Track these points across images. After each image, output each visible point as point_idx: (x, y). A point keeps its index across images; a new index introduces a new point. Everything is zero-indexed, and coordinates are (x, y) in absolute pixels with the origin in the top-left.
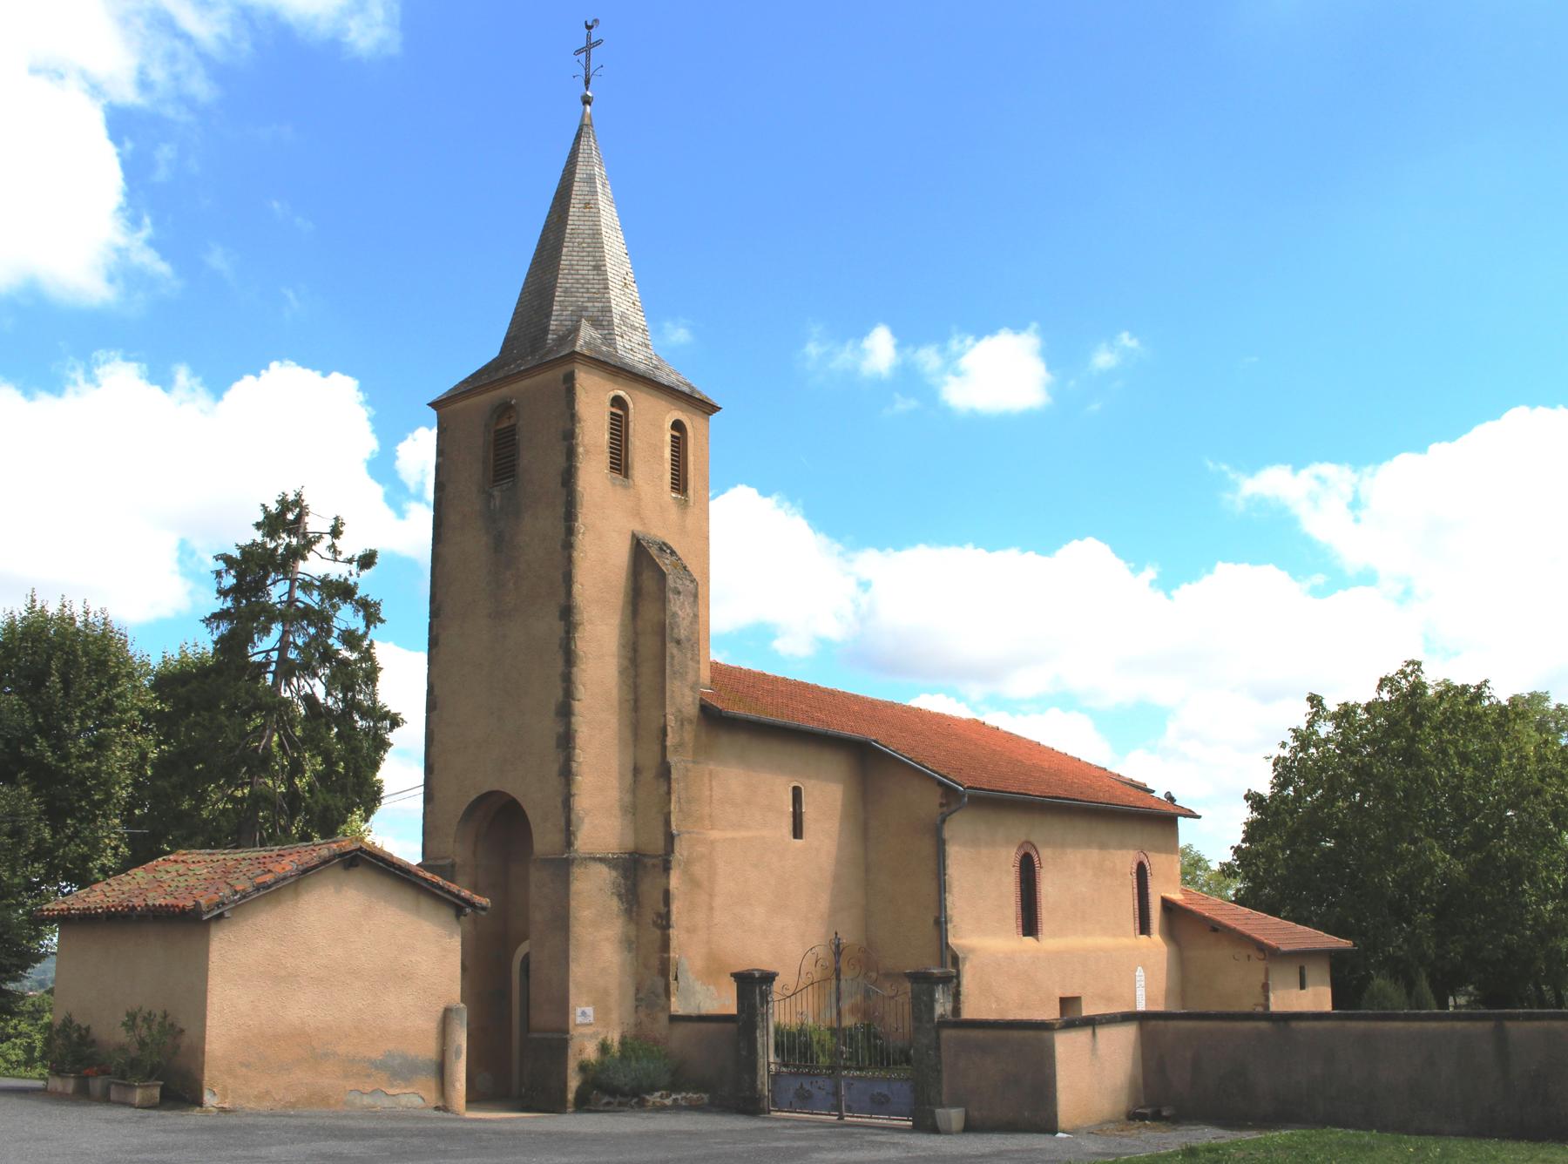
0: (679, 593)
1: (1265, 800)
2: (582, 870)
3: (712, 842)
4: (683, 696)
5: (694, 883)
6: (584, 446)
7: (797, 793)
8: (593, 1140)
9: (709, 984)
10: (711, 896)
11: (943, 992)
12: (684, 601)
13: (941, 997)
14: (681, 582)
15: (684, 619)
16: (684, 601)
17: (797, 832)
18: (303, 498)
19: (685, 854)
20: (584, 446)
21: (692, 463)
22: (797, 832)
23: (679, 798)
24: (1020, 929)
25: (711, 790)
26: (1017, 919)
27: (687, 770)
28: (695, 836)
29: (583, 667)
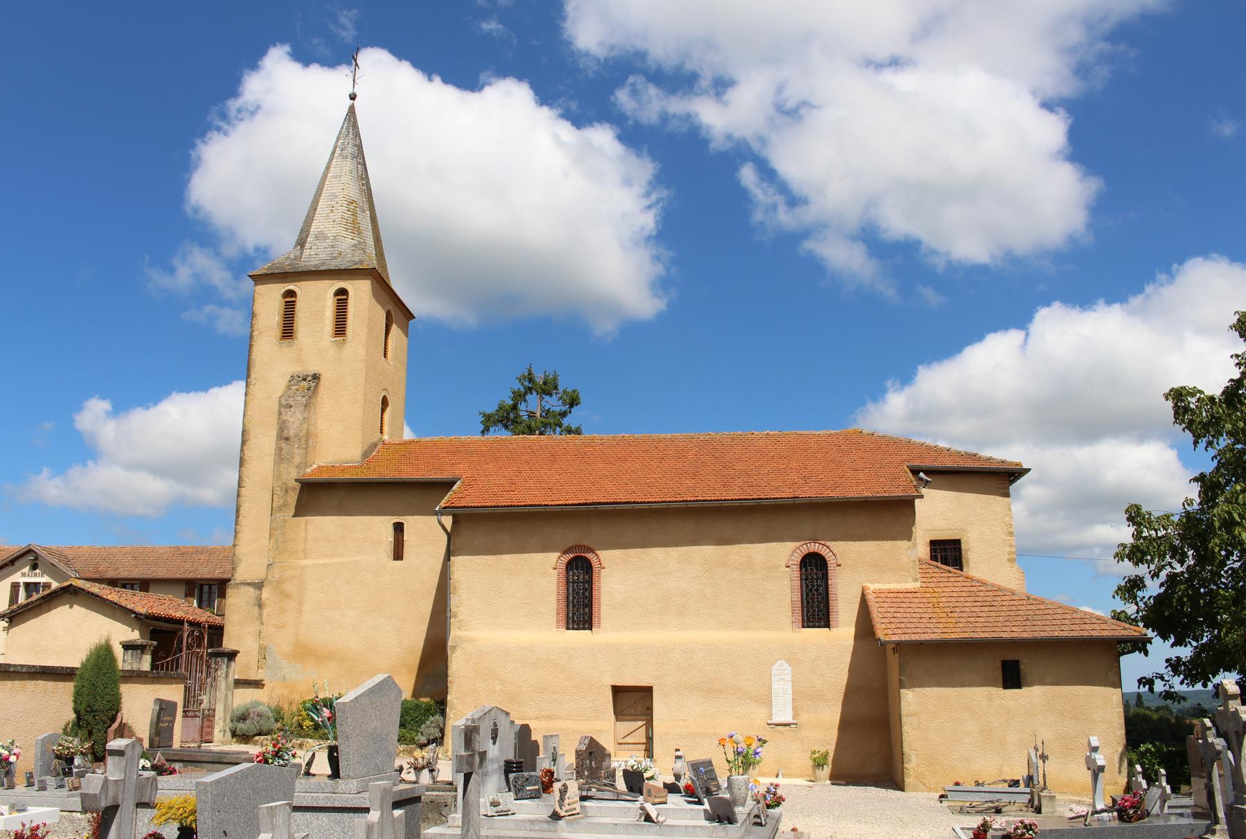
0: (291, 407)
1: (1206, 476)
2: (235, 591)
3: (302, 568)
4: (289, 473)
5: (285, 595)
6: (258, 330)
7: (399, 528)
8: (953, 829)
9: (295, 663)
10: (300, 603)
11: (132, 656)
12: (295, 411)
13: (130, 659)
14: (292, 399)
15: (293, 423)
16: (295, 411)
17: (398, 554)
18: (570, 390)
19: (277, 576)
20: (258, 330)
21: (352, 320)
22: (398, 554)
23: (277, 541)
24: (563, 617)
25: (306, 532)
26: (558, 614)
27: (285, 521)
28: (286, 564)
29: (248, 466)
